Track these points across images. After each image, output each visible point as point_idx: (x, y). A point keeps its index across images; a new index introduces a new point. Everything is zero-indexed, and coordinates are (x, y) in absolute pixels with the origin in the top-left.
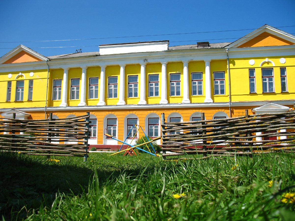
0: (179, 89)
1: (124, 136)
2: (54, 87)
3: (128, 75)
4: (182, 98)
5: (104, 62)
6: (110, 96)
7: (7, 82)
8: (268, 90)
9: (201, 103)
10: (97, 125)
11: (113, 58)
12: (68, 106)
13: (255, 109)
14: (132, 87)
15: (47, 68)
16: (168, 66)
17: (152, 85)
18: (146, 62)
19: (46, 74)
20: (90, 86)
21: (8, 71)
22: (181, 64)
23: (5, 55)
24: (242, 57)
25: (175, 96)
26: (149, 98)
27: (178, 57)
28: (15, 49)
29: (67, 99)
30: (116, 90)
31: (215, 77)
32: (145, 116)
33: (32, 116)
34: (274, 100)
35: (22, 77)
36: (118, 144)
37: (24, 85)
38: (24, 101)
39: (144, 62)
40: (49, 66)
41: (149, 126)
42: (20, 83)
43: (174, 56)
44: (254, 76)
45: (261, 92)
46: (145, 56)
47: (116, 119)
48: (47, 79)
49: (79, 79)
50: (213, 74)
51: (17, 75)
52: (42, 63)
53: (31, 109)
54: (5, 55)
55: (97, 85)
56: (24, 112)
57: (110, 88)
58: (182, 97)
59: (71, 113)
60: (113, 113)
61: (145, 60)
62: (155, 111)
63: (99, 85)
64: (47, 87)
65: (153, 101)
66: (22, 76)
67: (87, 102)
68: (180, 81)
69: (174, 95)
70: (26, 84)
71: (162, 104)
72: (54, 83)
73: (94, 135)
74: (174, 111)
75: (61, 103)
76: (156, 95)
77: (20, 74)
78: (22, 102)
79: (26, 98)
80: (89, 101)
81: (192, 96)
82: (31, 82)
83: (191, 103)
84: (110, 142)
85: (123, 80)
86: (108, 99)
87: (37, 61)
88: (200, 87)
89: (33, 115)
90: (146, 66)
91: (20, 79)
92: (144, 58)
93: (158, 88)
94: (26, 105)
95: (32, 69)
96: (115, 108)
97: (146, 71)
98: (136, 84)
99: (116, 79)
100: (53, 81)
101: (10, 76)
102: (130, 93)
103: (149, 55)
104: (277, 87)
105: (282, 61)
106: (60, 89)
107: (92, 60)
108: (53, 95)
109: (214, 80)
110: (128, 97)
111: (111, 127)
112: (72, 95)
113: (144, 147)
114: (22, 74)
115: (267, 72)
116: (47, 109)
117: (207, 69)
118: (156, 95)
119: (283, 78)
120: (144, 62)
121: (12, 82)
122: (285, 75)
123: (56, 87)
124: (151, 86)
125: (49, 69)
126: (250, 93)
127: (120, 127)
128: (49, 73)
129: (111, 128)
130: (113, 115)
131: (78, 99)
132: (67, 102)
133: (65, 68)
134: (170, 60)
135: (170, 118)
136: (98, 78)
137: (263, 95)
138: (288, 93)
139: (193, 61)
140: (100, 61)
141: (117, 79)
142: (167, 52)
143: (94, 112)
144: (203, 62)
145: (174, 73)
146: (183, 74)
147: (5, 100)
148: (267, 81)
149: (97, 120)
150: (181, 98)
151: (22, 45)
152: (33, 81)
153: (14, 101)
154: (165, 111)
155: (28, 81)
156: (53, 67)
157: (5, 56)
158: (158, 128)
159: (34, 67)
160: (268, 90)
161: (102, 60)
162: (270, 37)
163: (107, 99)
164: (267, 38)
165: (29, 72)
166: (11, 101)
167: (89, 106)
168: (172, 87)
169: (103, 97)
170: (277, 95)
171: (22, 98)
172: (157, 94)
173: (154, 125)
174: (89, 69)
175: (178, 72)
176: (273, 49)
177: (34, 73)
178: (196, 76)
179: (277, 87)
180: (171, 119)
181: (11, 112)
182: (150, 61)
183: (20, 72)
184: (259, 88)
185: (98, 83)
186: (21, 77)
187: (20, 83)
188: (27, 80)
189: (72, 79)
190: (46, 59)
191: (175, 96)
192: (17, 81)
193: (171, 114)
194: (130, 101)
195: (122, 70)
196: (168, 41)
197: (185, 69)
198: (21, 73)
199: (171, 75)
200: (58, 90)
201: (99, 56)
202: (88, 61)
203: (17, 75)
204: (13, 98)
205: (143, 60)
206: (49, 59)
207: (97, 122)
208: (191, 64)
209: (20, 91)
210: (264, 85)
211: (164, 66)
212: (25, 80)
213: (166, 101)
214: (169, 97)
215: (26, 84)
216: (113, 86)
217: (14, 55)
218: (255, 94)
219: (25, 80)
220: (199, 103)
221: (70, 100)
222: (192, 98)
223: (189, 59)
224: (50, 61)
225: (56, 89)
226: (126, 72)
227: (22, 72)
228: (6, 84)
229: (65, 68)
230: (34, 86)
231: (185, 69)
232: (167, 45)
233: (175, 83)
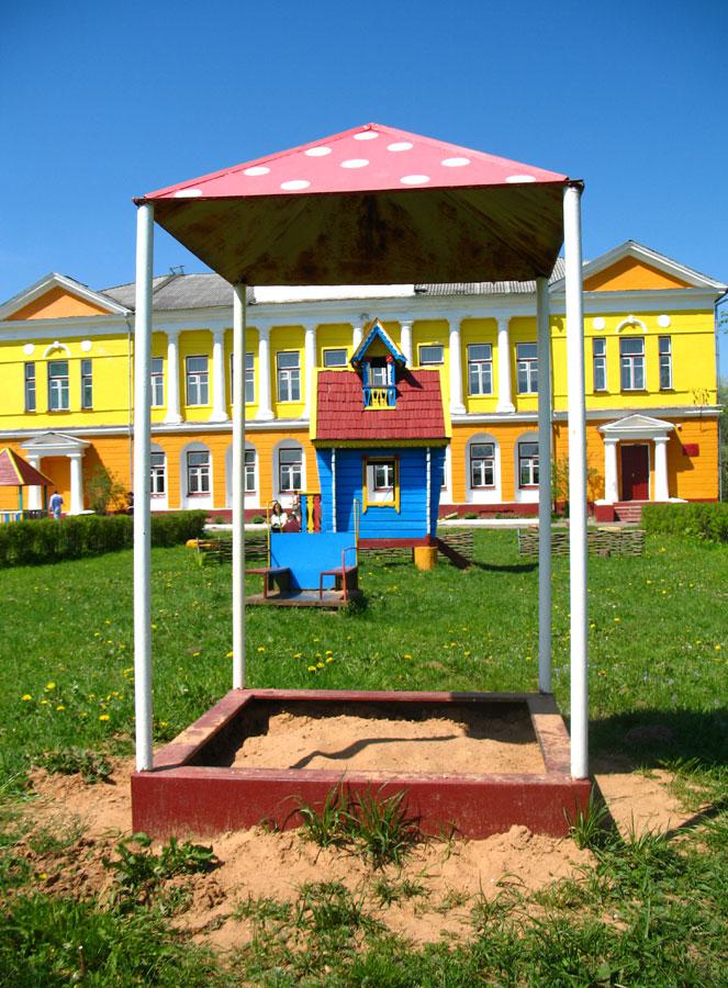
1: (181, 489)
3: (323, 349)
6: (284, 397)
7: (23, 364)
8: (56, 404)
9: (490, 414)
13: (605, 428)
16: (416, 328)
22: (442, 326)
24: (647, 310)
25: (290, 400)
31: (520, 355)
33: (95, 447)
34: (643, 407)
38: (71, 408)
45: (657, 389)
51: (49, 347)
60: (294, 436)
61: (364, 314)
66: (60, 350)
73: (205, 487)
76: (293, 399)
84: (480, 497)
87: (101, 313)
88: (296, 383)
89: (97, 444)
91: (56, 356)
93: (90, 389)
94: (78, 420)
99: (294, 358)
101: (29, 348)
104: (651, 379)
105: (663, 323)
114: (63, 345)
115: (631, 344)
117: (503, 337)
118: (293, 399)
119: (664, 359)
121: (37, 365)
126: (595, 391)
127: (501, 464)
129: (287, 469)
130: (295, 440)
134: (420, 316)
138: (672, 392)
141: (298, 358)
144: (493, 321)
145: (429, 344)
148: (631, 365)
160: (56, 404)
162: (639, 267)
164: (635, 269)
171: (65, 404)
172: (296, 395)
175: (437, 343)
178: (478, 350)
179: (651, 379)
183: (56, 340)
184: (612, 381)
193: (476, 436)
195: (310, 337)
197: (454, 338)
208: (466, 326)
210: (625, 373)
217: (33, 299)
218: (605, 394)
220: (484, 415)
226: (318, 342)
228: (20, 370)
230: (95, 374)
231: (454, 338)
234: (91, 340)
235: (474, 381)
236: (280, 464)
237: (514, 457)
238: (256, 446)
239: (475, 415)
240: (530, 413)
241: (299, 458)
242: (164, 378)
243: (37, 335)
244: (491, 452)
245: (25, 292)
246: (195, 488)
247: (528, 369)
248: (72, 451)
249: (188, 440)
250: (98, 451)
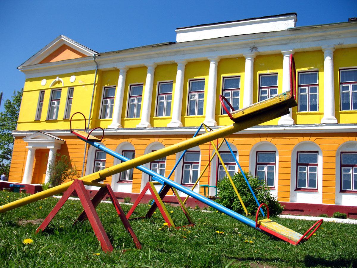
0: (316, 101)
2: (104, 98)
4: (321, 115)
5: (183, 54)
6: (192, 112)
10: (200, 161)
11: (200, 47)
12: (182, 126)
14: (266, 94)
15: (94, 69)
17: (305, 90)
18: (254, 53)
19: (92, 78)
20: (159, 96)
22: (319, 54)
23: (39, 51)
25: (308, 111)
26: (298, 114)
27: (315, 41)
28: (53, 42)
29: (122, 118)
30: (201, 103)
32: (250, 147)
35: (59, 84)
36: (132, 192)
37: (61, 96)
38: (58, 119)
39: (252, 51)
40: (97, 65)
41: (258, 166)
42: (56, 93)
43: (306, 38)
44: (317, 83)
46: (252, 42)
47: (199, 152)
48: (93, 85)
49: (143, 84)
50: (338, 72)
52: (87, 60)
53: (66, 132)
54: (39, 51)
55: (170, 95)
56: (57, 137)
57: (191, 98)
58: (320, 114)
59: (126, 140)
61: (254, 47)
62: (269, 139)
63: (173, 94)
64: (93, 97)
65: (160, 123)
66: (59, 82)
67: (151, 122)
68: (318, 85)
69: (307, 111)
70: (64, 94)
71: (157, 127)
72: (104, 93)
74: (306, 139)
75: (111, 124)
77: (57, 79)
78: (56, 121)
79: (61, 115)
81: (340, 111)
82: (71, 90)
83: (338, 124)
84: (302, 198)
85: (251, 79)
86: (186, 117)
88: (314, 97)
89: (69, 142)
90: (255, 59)
91: (57, 86)
92: (252, 45)
96: (180, 132)
97: (255, 69)
98: (274, 88)
99: (201, 84)
100: (189, 81)
101: (44, 81)
102: (191, 108)
103: (261, 37)
106: (113, 102)
107: (164, 51)
108: (101, 109)
109: (341, 83)
110: (221, 114)
111: (264, 167)
112: (130, 111)
113: (235, 199)
114: (61, 79)
120: (252, 51)
122: (317, 83)
123: (107, 98)
124: (263, 95)
125: (97, 70)
128: (98, 75)
129: (263, 168)
131: (170, 115)
132: (120, 121)
133: (122, 66)
134: (299, 46)
135: (298, 152)
136: (173, 82)
137: (46, 123)
139: (343, 47)
140: (176, 53)
142: (294, 32)
143: (162, 139)
146: (322, 70)
147: (33, 118)
149: (201, 153)
150: (319, 116)
151: (63, 36)
152: (73, 90)
153: (46, 120)
154: (289, 138)
156: (103, 67)
157: (40, 52)
158: (317, 172)
159: (77, 67)
161: (179, 51)
163: (186, 116)
165: (69, 75)
166: (41, 120)
167: (154, 128)
168: (301, 95)
169: (179, 113)
170: (59, 122)
173: (266, 164)
174: (129, 71)
177: (77, 77)
180: (299, 153)
181: (36, 137)
182: (263, 50)
185: (204, 89)
186: (58, 84)
187: (56, 93)
189: (190, 80)
190: (93, 54)
191: (308, 111)
192: (53, 90)
194: (158, 123)
195: (212, 66)
196: (296, 14)
197: (328, 62)
198: (59, 78)
199: (300, 75)
200: (109, 104)
201: (174, 44)
202: (158, 54)
203: (54, 80)
204: (44, 116)
205: (250, 49)
206: (98, 53)
207: (200, 156)
209: (55, 106)
211: (288, 58)
212: (62, 89)
213: (291, 120)
214: (297, 113)
215: (64, 94)
216: (165, 97)
219: (62, 89)
221: (125, 119)
222: (341, 115)
223: (336, 42)
224: (100, 57)
225: (106, 102)
226: (219, 71)
227: (60, 76)
229: (122, 66)
231: (328, 62)
232: (293, 20)
233: (307, 88)
234: (47, 79)
235: (345, 102)
236: (298, 164)
237: (335, 166)
238: (278, 148)
239: (345, 125)
240: (145, 128)
241: (274, 159)
242: (319, 88)
243: (49, 74)
244: (316, 159)
245: (46, 47)
246: (303, 183)
247: (350, 90)
248: (50, 144)
249: (122, 141)
250: (68, 147)
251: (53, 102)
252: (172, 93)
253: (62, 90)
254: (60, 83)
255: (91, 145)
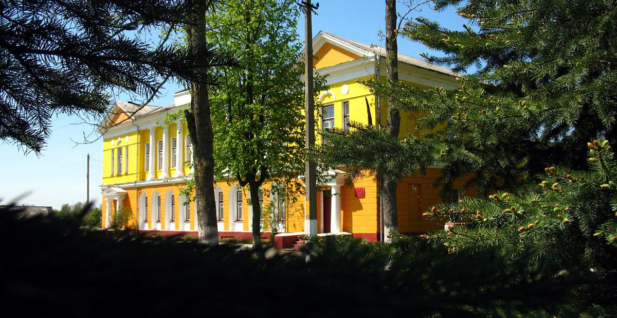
21: (339, 81)
35: (329, 97)
66: (120, 142)
77: (119, 139)
80: (171, 171)
82: (346, 104)
95: (126, 132)
116: (138, 184)
155: (340, 104)
156: (142, 128)
167: (159, 180)
176: (345, 67)
188: (337, 103)
192: (344, 103)
212: (350, 100)
251: (326, 122)
252: (333, 119)
253: (334, 106)
254: (331, 96)
255: (250, 185)
